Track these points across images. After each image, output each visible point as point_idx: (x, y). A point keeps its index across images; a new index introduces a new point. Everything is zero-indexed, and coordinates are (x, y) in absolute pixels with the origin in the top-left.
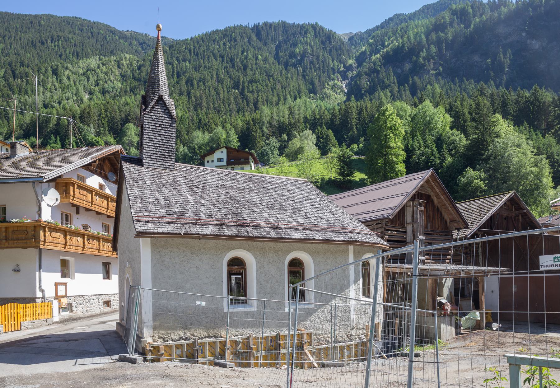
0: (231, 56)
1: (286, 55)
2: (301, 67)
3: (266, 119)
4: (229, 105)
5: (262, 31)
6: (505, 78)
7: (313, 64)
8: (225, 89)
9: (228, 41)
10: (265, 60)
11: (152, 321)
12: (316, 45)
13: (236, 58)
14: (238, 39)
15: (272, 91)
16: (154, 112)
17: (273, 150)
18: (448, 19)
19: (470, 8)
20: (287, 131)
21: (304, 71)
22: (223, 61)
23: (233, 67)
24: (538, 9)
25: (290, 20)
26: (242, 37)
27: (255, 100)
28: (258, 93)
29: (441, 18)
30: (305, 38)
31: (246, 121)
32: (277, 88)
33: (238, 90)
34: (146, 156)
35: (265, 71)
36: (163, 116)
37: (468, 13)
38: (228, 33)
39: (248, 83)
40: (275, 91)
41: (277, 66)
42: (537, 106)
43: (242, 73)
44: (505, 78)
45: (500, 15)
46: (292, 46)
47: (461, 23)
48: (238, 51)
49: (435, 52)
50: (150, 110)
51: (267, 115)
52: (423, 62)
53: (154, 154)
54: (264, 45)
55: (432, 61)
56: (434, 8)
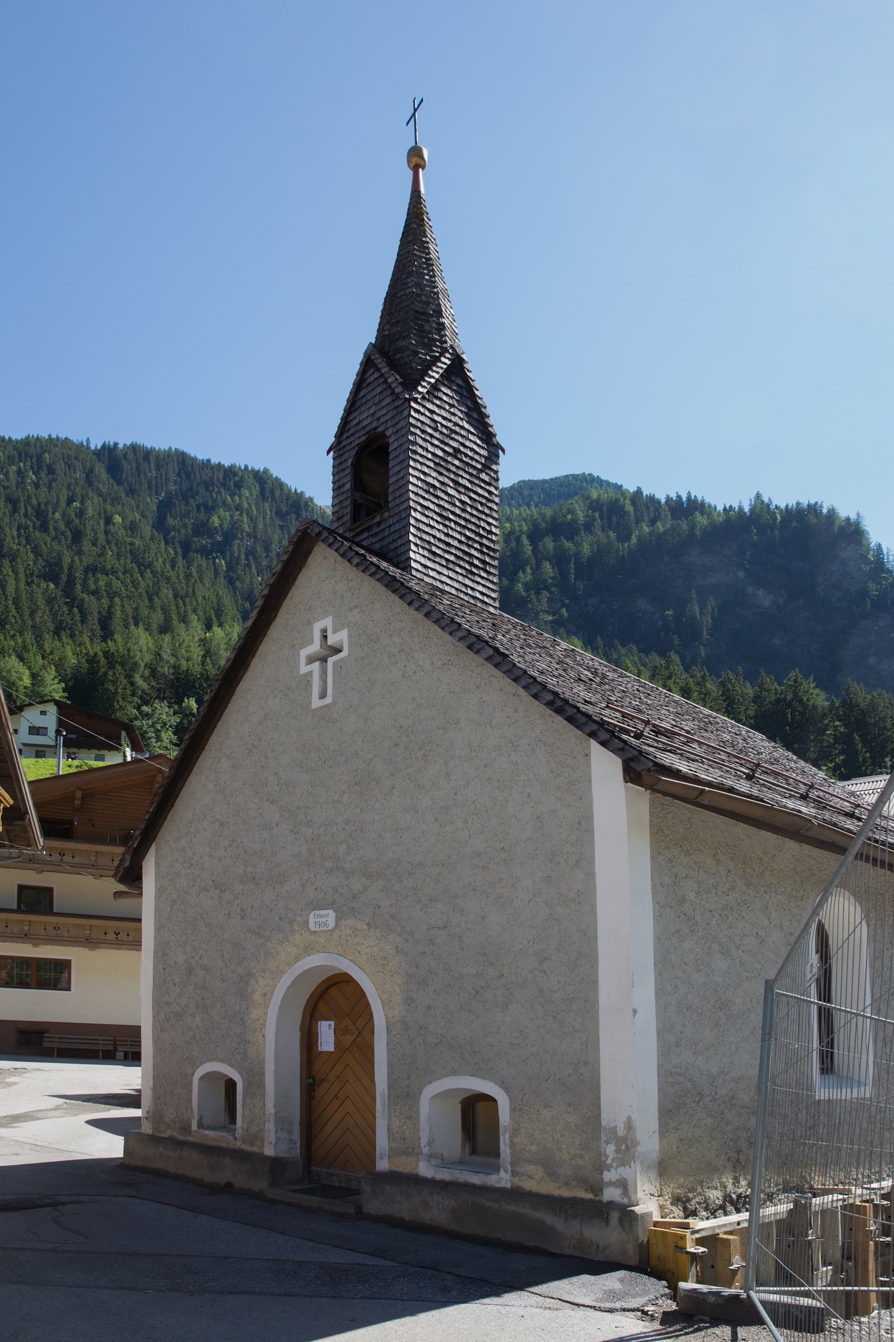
0: (39, 504)
1: (185, 526)
2: (224, 558)
3: (144, 658)
4: (33, 613)
5: (124, 462)
6: (703, 653)
7: (255, 558)
8: (22, 575)
9: (32, 468)
10: (132, 528)
11: (657, 1134)
12: (264, 518)
13: (51, 510)
14: (60, 467)
15: (151, 600)
16: (438, 402)
17: (159, 731)
18: (581, 516)
19: (628, 502)
20: (198, 693)
21: (231, 567)
22: (15, 510)
23: (44, 528)
24: (769, 531)
25: (199, 451)
26: (69, 465)
27: (104, 614)
28: (111, 599)
29: (565, 511)
30: (237, 497)
31: (87, 654)
32: (162, 595)
33: (57, 584)
34: (418, 542)
35: (131, 552)
36: (466, 426)
37: (625, 512)
38: (32, 450)
39: (86, 571)
40: (156, 600)
41: (163, 546)
42: (799, 711)
43: (69, 547)
44: (703, 653)
45: (693, 527)
46: (202, 509)
47: (610, 529)
48: (58, 495)
49: (552, 578)
50: (428, 392)
51: (145, 648)
52: (524, 594)
53: (440, 540)
54: (127, 495)
55: (545, 594)
56: (543, 490)
